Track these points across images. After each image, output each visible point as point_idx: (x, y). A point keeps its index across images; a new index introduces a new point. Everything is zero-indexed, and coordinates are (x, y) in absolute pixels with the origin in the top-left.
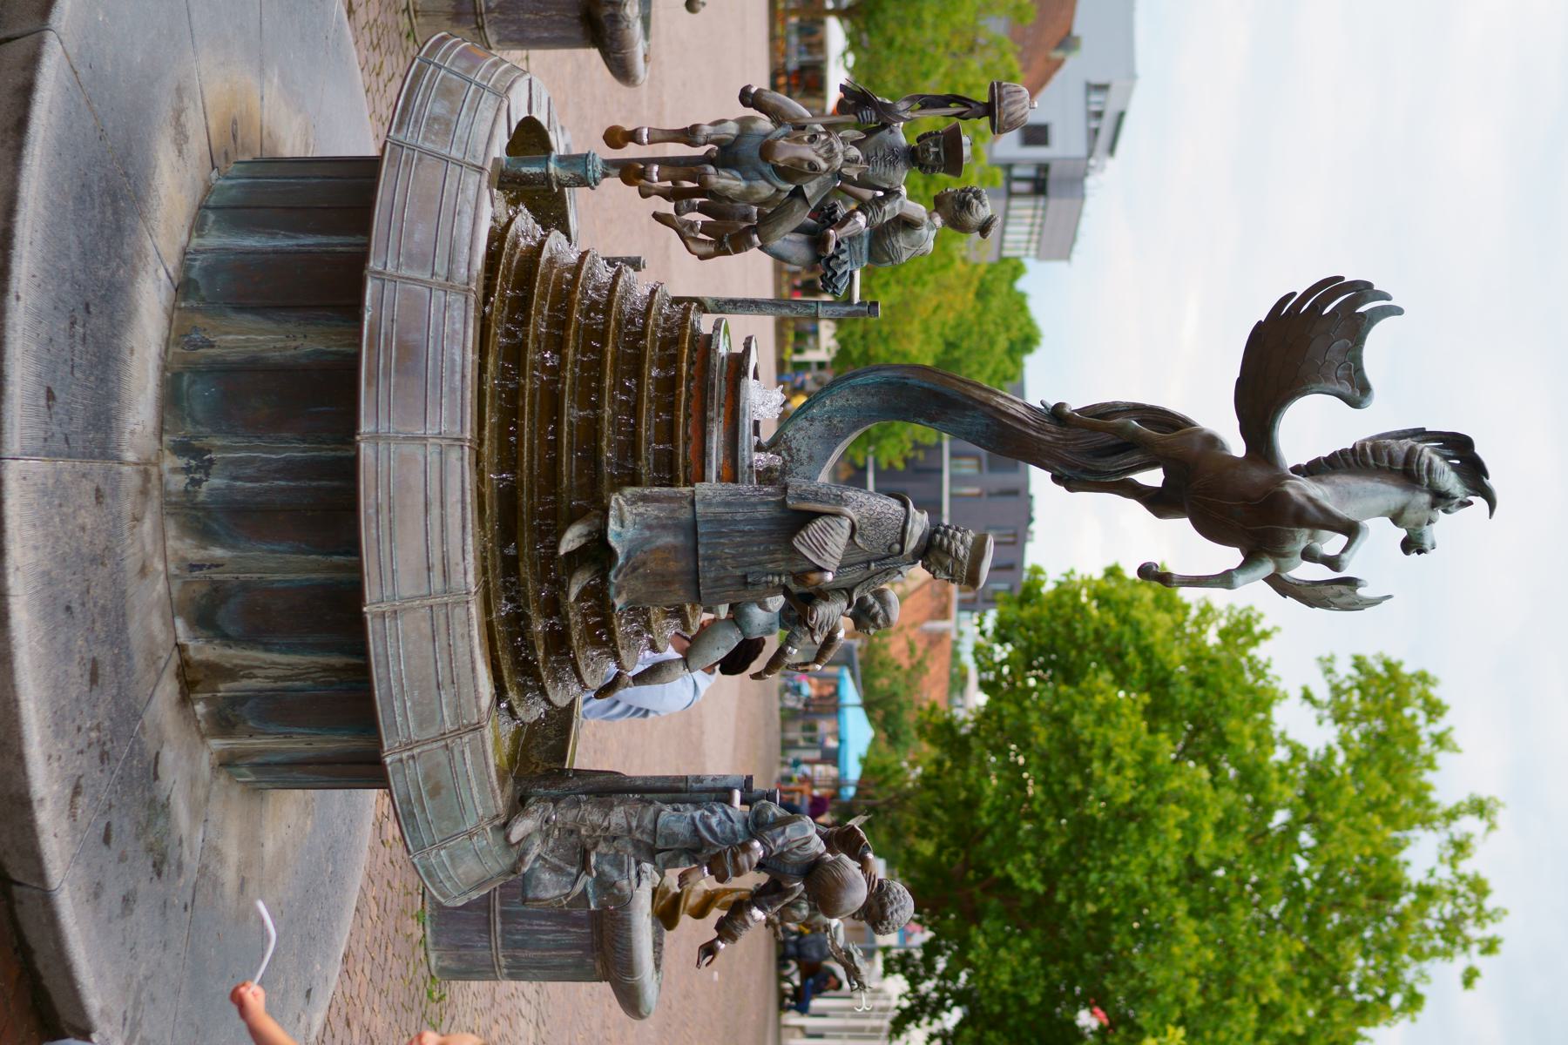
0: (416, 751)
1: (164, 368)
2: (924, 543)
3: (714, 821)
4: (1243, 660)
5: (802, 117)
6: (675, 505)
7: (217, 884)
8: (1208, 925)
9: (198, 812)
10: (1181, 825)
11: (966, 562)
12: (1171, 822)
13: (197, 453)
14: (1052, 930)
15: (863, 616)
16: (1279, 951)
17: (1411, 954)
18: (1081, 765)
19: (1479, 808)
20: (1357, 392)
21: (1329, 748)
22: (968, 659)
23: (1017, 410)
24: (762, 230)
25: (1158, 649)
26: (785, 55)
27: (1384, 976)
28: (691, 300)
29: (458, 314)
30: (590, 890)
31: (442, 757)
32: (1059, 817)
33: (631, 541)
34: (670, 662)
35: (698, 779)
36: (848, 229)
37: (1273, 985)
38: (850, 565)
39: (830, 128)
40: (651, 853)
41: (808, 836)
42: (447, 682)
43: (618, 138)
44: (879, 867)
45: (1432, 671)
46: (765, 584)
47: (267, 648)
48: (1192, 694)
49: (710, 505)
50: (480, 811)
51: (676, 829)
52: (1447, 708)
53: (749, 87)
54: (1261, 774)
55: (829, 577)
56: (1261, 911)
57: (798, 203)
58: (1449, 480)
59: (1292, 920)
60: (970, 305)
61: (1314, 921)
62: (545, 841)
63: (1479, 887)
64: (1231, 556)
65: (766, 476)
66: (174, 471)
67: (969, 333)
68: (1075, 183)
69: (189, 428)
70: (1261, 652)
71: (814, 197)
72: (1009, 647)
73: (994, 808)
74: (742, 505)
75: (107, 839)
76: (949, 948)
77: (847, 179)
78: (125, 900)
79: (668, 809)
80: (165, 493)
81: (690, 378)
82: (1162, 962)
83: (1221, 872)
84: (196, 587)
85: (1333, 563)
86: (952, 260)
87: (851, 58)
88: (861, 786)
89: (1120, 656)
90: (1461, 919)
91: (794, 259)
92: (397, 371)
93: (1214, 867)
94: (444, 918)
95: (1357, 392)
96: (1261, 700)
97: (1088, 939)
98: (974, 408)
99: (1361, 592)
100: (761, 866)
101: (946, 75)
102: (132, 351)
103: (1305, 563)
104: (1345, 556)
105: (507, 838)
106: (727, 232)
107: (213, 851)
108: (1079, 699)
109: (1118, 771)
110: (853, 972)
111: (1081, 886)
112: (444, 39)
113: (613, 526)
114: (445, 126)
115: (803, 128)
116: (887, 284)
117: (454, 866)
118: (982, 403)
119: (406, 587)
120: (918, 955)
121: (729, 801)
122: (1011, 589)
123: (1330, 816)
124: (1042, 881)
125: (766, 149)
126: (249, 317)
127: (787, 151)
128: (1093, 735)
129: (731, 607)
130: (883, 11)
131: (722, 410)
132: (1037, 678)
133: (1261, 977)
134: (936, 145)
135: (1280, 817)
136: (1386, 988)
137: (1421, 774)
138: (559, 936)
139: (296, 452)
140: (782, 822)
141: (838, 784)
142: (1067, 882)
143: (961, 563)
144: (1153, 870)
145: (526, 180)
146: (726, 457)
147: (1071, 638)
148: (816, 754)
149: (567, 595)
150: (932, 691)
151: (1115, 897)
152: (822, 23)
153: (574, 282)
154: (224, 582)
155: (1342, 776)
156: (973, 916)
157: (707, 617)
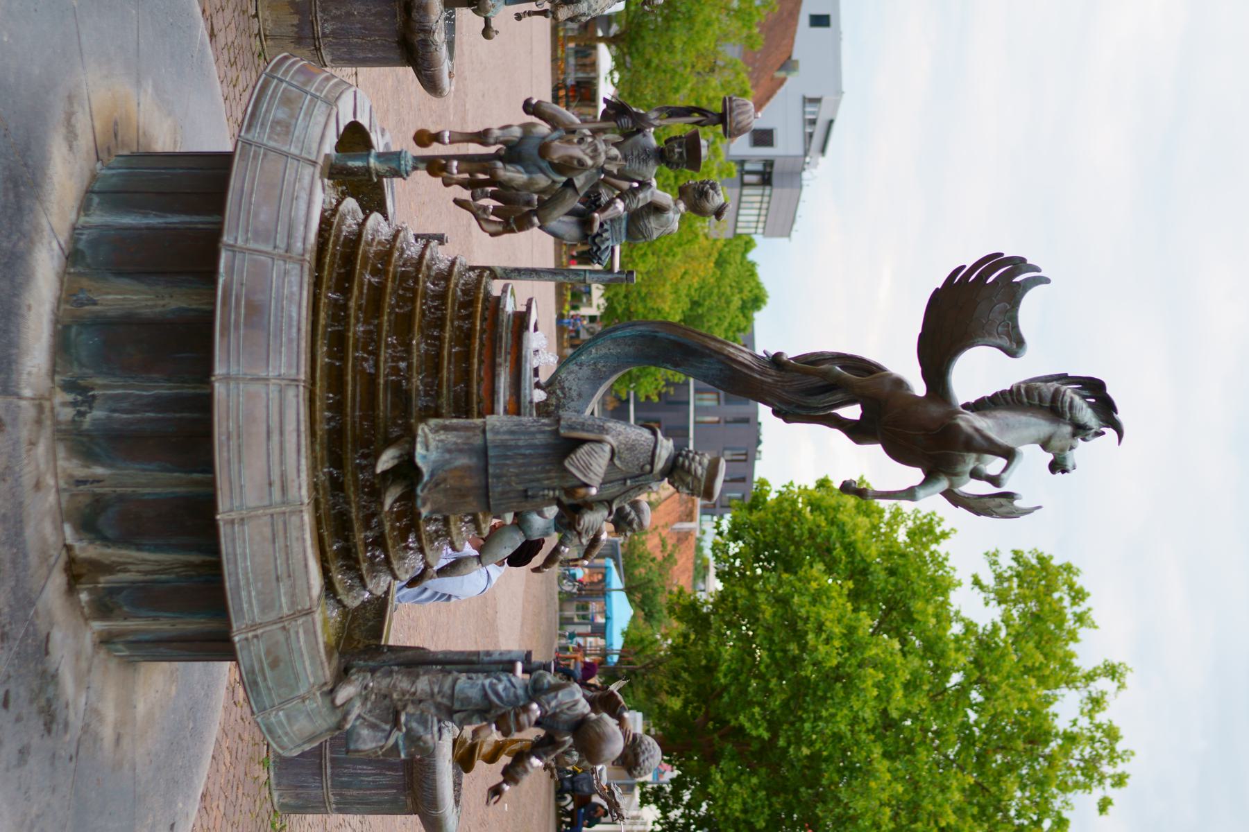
0: (259, 632)
1: (56, 322)
2: (670, 464)
3: (500, 688)
4: (927, 553)
5: (573, 123)
6: (470, 434)
7: (97, 739)
8: (898, 765)
9: (82, 680)
10: (877, 685)
11: (703, 480)
12: (870, 682)
13: (83, 390)
14: (774, 768)
15: (621, 522)
16: (955, 784)
17: (1058, 787)
18: (800, 637)
19: (1112, 671)
20: (1014, 345)
21: (994, 625)
22: (708, 553)
23: (745, 358)
24: (541, 213)
25: (859, 545)
26: (564, 73)
27: (1037, 804)
28: (484, 269)
29: (295, 279)
30: (401, 743)
31: (281, 637)
32: (781, 678)
33: (434, 462)
34: (468, 558)
35: (488, 653)
36: (610, 213)
37: (950, 812)
38: (611, 482)
39: (595, 132)
40: (450, 713)
41: (576, 699)
42: (285, 575)
43: (425, 138)
44: (636, 721)
45: (1075, 565)
46: (539, 496)
47: (139, 548)
48: (886, 582)
49: (498, 433)
50: (312, 680)
52: (1088, 595)
53: (530, 99)
54: (941, 645)
55: (594, 491)
56: (940, 753)
57: (570, 192)
58: (1087, 415)
59: (965, 760)
60: (711, 272)
61: (982, 761)
62: (364, 704)
63: (1112, 734)
64: (915, 475)
65: (542, 409)
66: (64, 404)
67: (711, 294)
68: (794, 176)
69: (76, 370)
70: (941, 548)
71: (583, 186)
72: (741, 543)
73: (730, 670)
74: (524, 433)
75: (6, 704)
76: (692, 783)
77: (609, 173)
78: (21, 752)
79: (463, 677)
80: (56, 423)
81: (483, 331)
82: (862, 795)
83: (908, 723)
84: (80, 498)
85: (995, 480)
86: (697, 236)
87: (617, 75)
88: (623, 654)
89: (829, 551)
90: (1097, 759)
91: (567, 236)
92: (245, 325)
93: (903, 718)
94: (284, 766)
95: (1014, 345)
96: (940, 586)
97: (804, 775)
98: (710, 356)
99: (1017, 503)
100: (538, 723)
101: (692, 90)
102: (29, 307)
103: (973, 481)
104: (1004, 475)
105: (333, 701)
106: (513, 215)
107: (94, 712)
108: (798, 584)
109: (827, 641)
110: (614, 806)
111: (798, 733)
112: (286, 58)
113: (420, 450)
114: (285, 128)
115: (573, 132)
116: (645, 254)
117: (291, 725)
118: (716, 352)
119: (251, 499)
120: (668, 789)
121: (512, 670)
122: (743, 497)
123: (996, 679)
124: (767, 730)
125: (544, 148)
126: (126, 280)
127: (560, 151)
128: (808, 612)
129: (516, 515)
130: (643, 38)
131: (509, 357)
132: (763, 568)
133: (940, 806)
134: (680, 147)
135: (956, 678)
136: (1039, 815)
137: (1067, 644)
138: (378, 778)
139: (164, 389)
140: (556, 688)
141: (605, 653)
142: (786, 731)
143: (699, 480)
144: (854, 721)
145: (351, 172)
146: (511, 395)
147: (790, 538)
148: (589, 629)
149: (382, 504)
150: (680, 579)
151: (825, 743)
152: (595, 48)
153: (389, 253)
154: (104, 494)
155: (1005, 647)
156: (713, 758)
157: (495, 521)
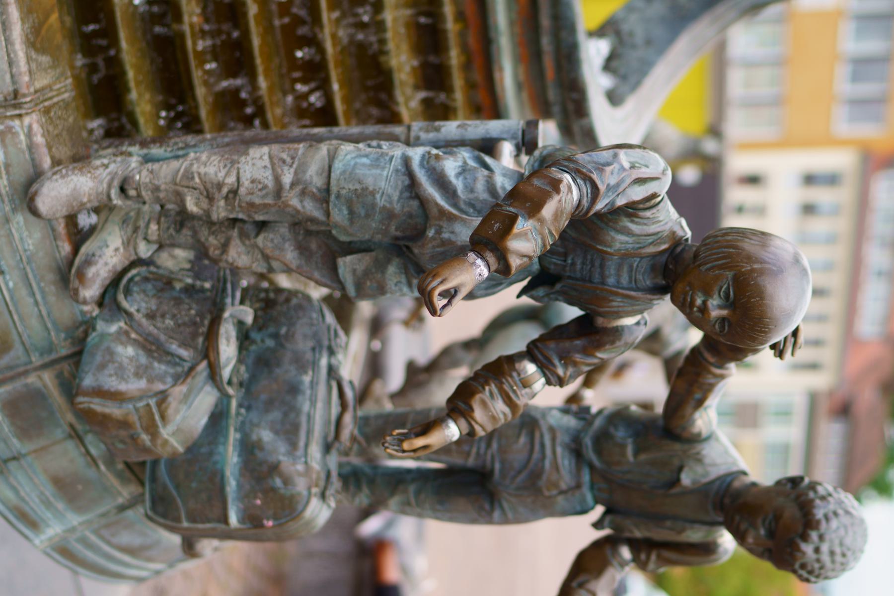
51: (369, 182)
